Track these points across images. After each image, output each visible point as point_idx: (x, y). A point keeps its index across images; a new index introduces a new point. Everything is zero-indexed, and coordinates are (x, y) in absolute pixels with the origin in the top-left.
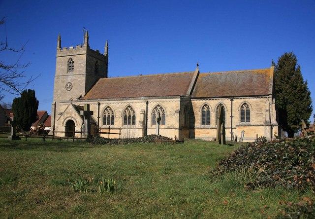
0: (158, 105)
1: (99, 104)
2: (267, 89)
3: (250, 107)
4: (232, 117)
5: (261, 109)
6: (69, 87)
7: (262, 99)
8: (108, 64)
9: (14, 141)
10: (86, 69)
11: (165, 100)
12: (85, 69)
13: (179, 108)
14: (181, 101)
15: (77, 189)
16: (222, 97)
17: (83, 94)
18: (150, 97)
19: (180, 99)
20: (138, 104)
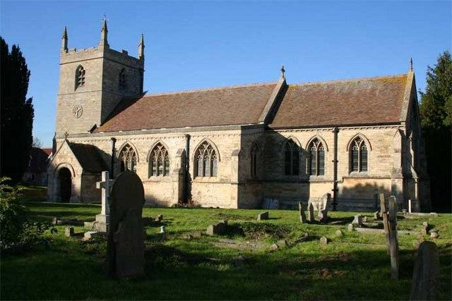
0: (205, 143)
1: (114, 140)
2: (398, 112)
3: (367, 144)
4: (336, 162)
5: (386, 148)
6: (78, 112)
7: (389, 130)
8: (145, 74)
9: (281, 156)
10: (104, 83)
11: (230, 132)
12: (101, 82)
13: (239, 148)
14: (242, 135)
15: (189, 238)
16: (319, 127)
17: (99, 124)
18: (195, 126)
19: (240, 132)
20: (173, 141)
